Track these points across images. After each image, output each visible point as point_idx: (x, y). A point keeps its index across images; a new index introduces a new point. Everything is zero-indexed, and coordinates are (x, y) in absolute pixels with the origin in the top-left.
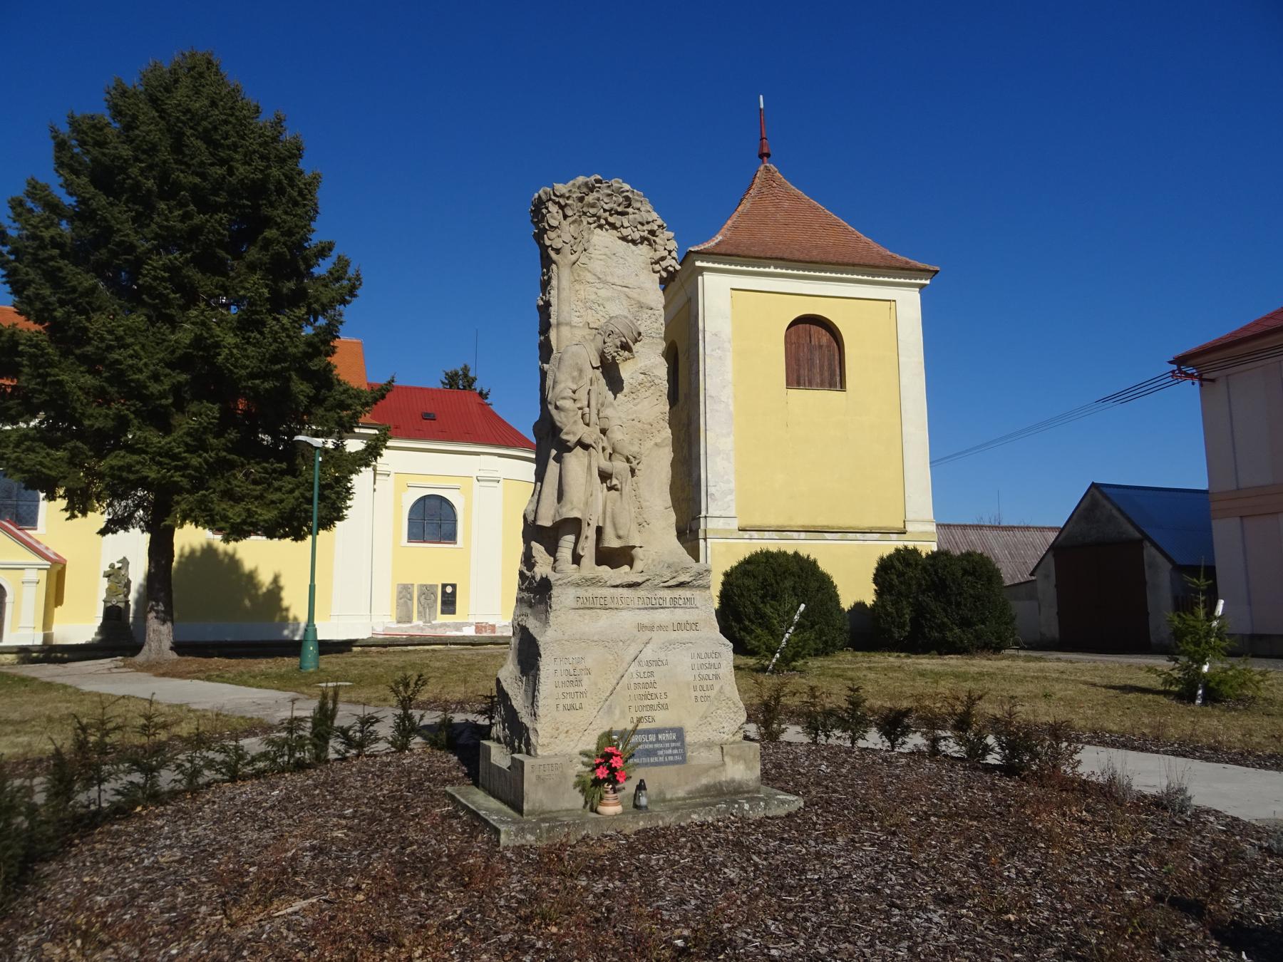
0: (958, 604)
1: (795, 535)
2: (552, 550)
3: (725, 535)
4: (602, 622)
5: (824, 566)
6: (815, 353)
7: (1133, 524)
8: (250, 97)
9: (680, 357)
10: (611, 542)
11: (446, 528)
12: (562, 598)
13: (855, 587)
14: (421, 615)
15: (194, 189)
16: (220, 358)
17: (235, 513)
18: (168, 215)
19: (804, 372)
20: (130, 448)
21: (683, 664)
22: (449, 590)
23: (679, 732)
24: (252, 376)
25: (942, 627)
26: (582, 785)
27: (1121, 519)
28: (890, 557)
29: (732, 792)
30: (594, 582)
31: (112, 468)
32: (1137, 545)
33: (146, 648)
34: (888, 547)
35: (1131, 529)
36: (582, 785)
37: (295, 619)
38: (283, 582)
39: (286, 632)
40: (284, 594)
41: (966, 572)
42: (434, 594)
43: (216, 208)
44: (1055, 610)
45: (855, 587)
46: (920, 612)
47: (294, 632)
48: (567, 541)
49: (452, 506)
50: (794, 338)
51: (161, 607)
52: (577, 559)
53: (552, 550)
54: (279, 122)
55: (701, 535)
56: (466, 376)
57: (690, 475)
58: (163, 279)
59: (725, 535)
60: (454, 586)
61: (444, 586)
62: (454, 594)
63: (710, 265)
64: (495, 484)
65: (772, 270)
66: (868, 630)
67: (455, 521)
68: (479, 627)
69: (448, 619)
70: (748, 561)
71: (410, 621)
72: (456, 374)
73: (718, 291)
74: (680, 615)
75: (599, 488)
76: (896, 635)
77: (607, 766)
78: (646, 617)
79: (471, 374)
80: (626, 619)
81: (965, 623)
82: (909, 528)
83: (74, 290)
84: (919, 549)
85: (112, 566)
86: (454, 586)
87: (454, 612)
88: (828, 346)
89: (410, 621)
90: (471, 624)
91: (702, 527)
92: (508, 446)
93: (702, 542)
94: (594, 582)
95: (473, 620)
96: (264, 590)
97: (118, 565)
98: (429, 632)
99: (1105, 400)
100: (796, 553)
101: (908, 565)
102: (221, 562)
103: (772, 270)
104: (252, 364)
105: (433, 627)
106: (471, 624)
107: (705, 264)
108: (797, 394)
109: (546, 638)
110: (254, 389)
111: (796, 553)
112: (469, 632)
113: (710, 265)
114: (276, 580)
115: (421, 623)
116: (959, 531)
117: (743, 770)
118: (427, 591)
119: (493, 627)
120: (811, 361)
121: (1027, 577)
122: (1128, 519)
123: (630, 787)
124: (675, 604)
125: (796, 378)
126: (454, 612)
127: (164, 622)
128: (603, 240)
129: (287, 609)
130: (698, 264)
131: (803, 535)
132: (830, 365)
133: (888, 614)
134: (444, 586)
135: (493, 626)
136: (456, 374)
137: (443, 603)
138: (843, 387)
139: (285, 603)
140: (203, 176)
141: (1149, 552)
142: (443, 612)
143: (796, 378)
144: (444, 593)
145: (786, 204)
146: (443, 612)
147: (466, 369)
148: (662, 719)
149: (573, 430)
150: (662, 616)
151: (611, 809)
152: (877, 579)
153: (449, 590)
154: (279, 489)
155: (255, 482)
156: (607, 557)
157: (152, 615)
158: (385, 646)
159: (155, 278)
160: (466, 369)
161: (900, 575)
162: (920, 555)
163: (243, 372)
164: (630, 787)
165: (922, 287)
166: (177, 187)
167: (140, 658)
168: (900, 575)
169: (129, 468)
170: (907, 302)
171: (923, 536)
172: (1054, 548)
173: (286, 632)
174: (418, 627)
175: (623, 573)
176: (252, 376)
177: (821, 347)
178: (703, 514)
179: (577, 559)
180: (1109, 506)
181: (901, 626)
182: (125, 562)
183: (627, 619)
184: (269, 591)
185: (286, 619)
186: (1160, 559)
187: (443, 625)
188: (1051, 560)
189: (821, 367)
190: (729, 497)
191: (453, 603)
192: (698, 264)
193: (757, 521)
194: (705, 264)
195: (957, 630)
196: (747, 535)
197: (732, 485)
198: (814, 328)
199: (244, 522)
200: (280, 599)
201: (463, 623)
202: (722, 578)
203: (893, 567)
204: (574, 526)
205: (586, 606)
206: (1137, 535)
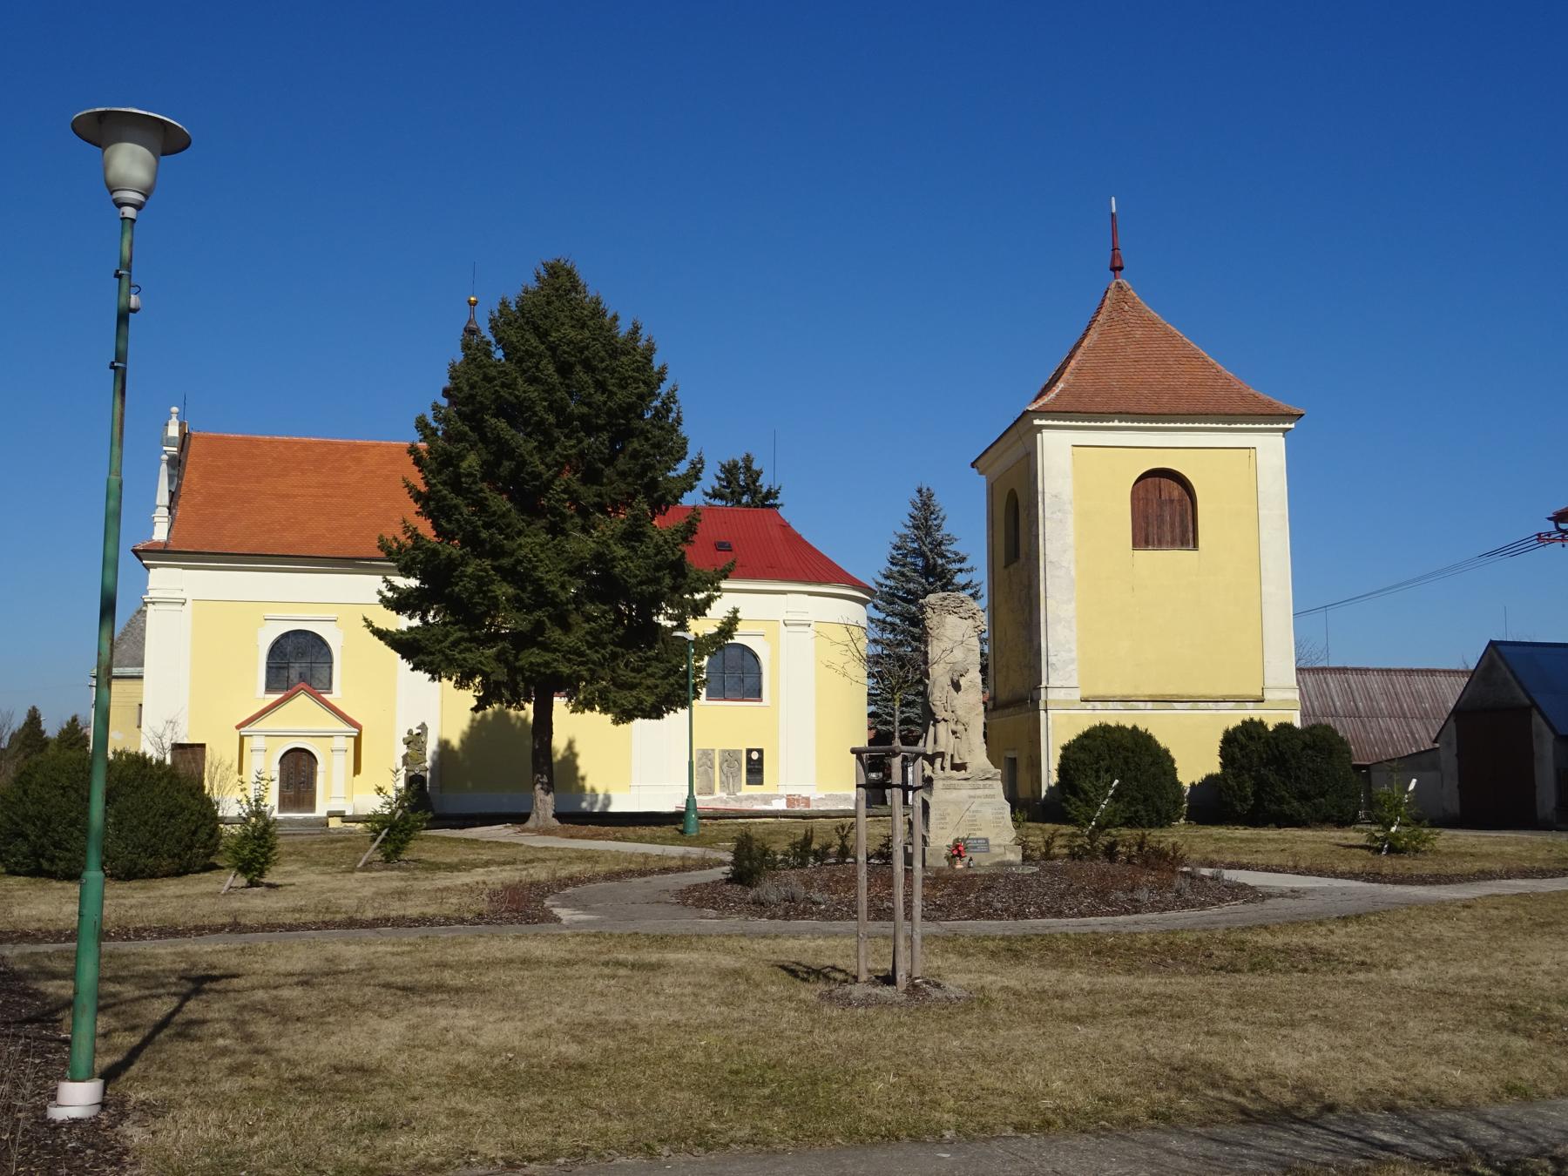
0: (1297, 778)
1: (1141, 705)
2: (932, 764)
3: (1066, 706)
4: (953, 795)
5: (1163, 741)
6: (1164, 511)
7: (1524, 690)
8: (611, 307)
9: (1021, 510)
10: (957, 761)
11: (749, 681)
12: (937, 785)
13: (1196, 760)
14: (724, 786)
15: (582, 417)
16: (617, 570)
17: (627, 699)
18: (566, 445)
19: (1153, 530)
20: (545, 647)
21: (988, 813)
22: (755, 756)
23: (987, 840)
24: (641, 583)
25: (1280, 800)
26: (947, 858)
27: (1514, 683)
28: (1235, 729)
29: (1011, 864)
30: (950, 778)
31: (531, 664)
32: (1524, 712)
33: (534, 816)
34: (1234, 717)
35: (1522, 695)
36: (947, 858)
37: (593, 790)
38: (578, 748)
39: (584, 805)
40: (580, 762)
41: (1306, 746)
42: (739, 761)
43: (600, 429)
44: (1456, 783)
45: (1196, 760)
46: (1261, 785)
47: (592, 804)
48: (939, 760)
49: (755, 656)
50: (1141, 494)
51: (545, 779)
52: (943, 768)
53: (932, 764)
54: (636, 329)
55: (1042, 706)
56: (748, 468)
57: (1031, 640)
58: (565, 501)
59: (1066, 706)
60: (760, 751)
61: (749, 751)
62: (760, 760)
63: (1050, 422)
64: (806, 629)
65: (1116, 423)
66: (1212, 804)
67: (760, 674)
68: (791, 800)
69: (755, 790)
70: (1086, 735)
71: (711, 792)
72: (735, 465)
73: (1060, 452)
74: (987, 792)
75: (952, 737)
76: (1239, 808)
77: (957, 851)
78: (972, 793)
79: (755, 467)
80: (964, 793)
81: (1304, 797)
82: (1267, 696)
83: (494, 513)
84: (1265, 720)
85: (410, 732)
86: (760, 751)
87: (761, 783)
88: (1180, 501)
89: (711, 792)
90: (781, 797)
91: (1043, 697)
92: (819, 582)
93: (1042, 713)
94: (950, 778)
95: (783, 791)
96: (559, 757)
97: (416, 731)
98: (734, 806)
99: (1489, 554)
100: (1135, 728)
101: (1251, 738)
102: (514, 726)
103: (1116, 423)
104: (642, 574)
105: (739, 800)
106: (781, 797)
107: (1043, 422)
108: (1142, 555)
109: (931, 801)
110: (641, 594)
111: (1135, 728)
112: (780, 805)
113: (1050, 422)
114: (570, 745)
115: (724, 795)
116: (1402, 678)
117: (1015, 856)
118: (729, 757)
119: (807, 800)
120: (1160, 517)
121: (1428, 745)
122: (1520, 683)
123: (966, 860)
124: (985, 787)
125: (1145, 536)
126: (761, 783)
127: (547, 792)
128: (951, 619)
129: (583, 779)
130: (1037, 422)
131: (1150, 705)
132: (1182, 521)
133: (1230, 788)
134: (749, 751)
135: (808, 799)
136: (735, 465)
137: (749, 771)
138: (1195, 546)
139: (581, 772)
140: (589, 405)
141: (1537, 719)
142: (749, 782)
143: (1145, 536)
144: (749, 760)
145: (1138, 334)
146: (749, 782)
147: (748, 460)
148: (979, 834)
149: (940, 714)
150: (979, 792)
151: (959, 866)
152: (1224, 753)
153: (755, 756)
154: (652, 675)
155: (633, 670)
156: (955, 767)
157: (538, 786)
158: (715, 818)
159: (557, 501)
160: (748, 460)
161: (1242, 748)
162: (1265, 728)
163: (633, 581)
164: (966, 860)
165: (1285, 431)
166: (571, 417)
167: (530, 824)
168: (1242, 748)
169: (547, 664)
170: (1278, 441)
171: (1284, 705)
172: (1460, 713)
173: (584, 805)
174: (721, 800)
175: (962, 774)
176: (641, 583)
177: (1172, 501)
178: (1044, 684)
179: (943, 768)
180: (1504, 668)
181: (1245, 799)
182: (423, 727)
183: (964, 793)
184: (565, 759)
185: (583, 789)
186: (1545, 728)
187: (748, 797)
188: (1452, 724)
189: (1172, 525)
190: (1071, 667)
191: (760, 771)
192: (1037, 422)
193: (1101, 690)
194: (1043, 422)
195: (1296, 804)
196: (1089, 705)
197: (1074, 655)
198: (1165, 482)
199: (635, 708)
200: (576, 768)
201: (773, 794)
202: (1060, 752)
203: (1236, 740)
204: (942, 755)
205: (947, 788)
206: (1527, 702)
